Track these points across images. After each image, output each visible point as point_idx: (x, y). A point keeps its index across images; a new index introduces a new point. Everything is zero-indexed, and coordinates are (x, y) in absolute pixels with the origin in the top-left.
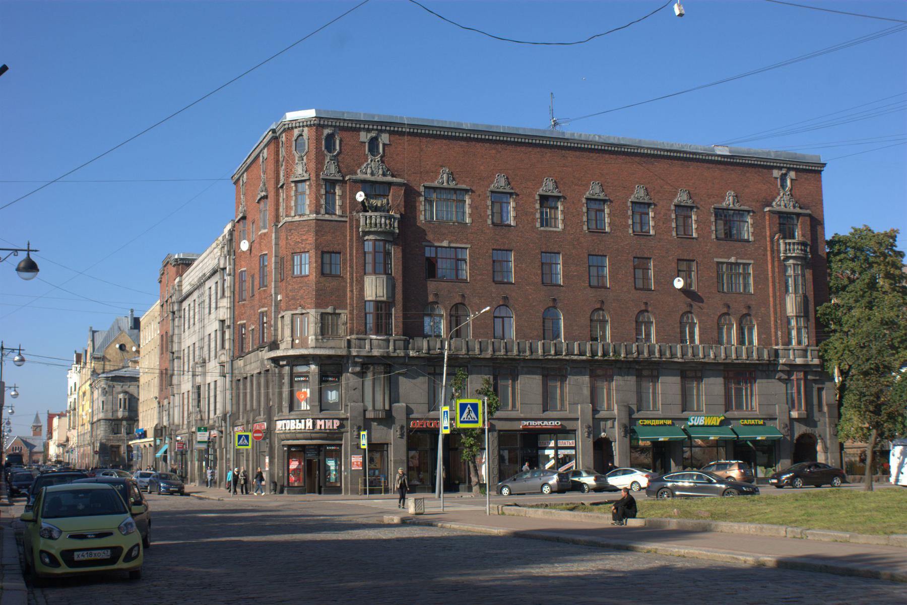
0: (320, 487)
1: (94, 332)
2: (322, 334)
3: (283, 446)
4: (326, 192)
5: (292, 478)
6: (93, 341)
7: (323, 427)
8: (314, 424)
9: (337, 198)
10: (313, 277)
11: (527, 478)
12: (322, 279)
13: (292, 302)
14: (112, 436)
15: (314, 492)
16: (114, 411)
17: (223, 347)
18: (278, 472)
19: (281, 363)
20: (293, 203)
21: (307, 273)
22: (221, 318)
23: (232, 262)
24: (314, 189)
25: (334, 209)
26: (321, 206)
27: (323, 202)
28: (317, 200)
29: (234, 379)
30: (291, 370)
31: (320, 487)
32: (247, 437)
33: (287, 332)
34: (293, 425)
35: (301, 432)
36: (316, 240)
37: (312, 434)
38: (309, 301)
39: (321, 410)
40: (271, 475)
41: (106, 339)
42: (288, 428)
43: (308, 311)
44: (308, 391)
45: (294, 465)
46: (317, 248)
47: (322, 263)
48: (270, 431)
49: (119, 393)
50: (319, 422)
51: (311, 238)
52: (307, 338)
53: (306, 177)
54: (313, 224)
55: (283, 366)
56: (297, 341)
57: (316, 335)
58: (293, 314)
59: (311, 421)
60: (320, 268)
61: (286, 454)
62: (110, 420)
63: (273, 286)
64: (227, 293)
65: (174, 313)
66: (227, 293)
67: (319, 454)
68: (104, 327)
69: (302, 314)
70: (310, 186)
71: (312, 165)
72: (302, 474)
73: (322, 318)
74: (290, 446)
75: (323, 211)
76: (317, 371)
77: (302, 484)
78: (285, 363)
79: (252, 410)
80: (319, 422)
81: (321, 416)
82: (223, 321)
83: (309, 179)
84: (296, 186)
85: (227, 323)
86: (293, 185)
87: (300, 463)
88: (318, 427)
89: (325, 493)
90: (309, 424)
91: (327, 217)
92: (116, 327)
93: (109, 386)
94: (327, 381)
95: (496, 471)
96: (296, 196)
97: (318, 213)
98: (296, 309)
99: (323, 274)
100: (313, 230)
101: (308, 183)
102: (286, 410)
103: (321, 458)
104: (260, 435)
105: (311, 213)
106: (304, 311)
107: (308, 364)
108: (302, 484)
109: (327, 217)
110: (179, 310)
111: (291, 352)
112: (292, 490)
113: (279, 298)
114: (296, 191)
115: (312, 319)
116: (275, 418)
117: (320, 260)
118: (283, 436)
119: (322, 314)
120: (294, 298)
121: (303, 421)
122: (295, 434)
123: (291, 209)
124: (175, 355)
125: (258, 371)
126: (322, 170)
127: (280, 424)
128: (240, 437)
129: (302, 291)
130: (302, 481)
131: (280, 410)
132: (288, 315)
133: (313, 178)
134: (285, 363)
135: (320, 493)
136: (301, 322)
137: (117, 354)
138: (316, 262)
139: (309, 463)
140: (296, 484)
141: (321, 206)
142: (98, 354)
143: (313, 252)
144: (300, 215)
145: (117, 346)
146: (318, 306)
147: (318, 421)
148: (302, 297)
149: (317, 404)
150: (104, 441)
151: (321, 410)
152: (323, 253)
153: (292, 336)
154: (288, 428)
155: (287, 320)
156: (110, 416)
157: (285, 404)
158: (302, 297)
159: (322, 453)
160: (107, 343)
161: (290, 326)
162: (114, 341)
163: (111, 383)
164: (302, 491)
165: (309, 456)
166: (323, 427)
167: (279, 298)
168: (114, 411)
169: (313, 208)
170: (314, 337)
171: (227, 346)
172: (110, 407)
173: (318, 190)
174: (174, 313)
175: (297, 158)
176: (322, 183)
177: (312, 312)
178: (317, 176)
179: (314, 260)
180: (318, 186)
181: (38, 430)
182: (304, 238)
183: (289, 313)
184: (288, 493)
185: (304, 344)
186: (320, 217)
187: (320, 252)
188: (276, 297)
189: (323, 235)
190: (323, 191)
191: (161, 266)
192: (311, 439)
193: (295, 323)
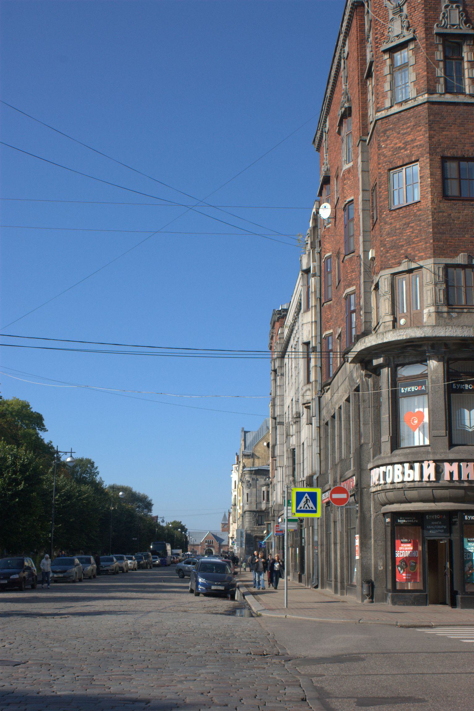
0: (454, 594)
1: (246, 432)
2: (448, 303)
3: (384, 514)
4: (446, 57)
5: (402, 575)
6: (245, 440)
7: (456, 477)
8: (439, 472)
9: (466, 65)
10: (427, 204)
11: (122, 570)
12: (445, 205)
13: (392, 253)
14: (256, 527)
15: (444, 603)
16: (258, 503)
17: (308, 382)
18: (377, 563)
19: (375, 362)
20: (387, 87)
21: (417, 198)
22: (305, 340)
23: (317, 256)
24: (423, 53)
25: (460, 79)
26: (436, 80)
27: (440, 72)
28: (430, 69)
29: (323, 423)
30: (394, 374)
31: (454, 594)
32: (313, 496)
33: (385, 306)
34: (400, 474)
35: (413, 486)
36: (430, 137)
37: (433, 490)
38: (422, 245)
39: (451, 445)
40: (365, 569)
41: (255, 438)
42: (389, 480)
43: (421, 263)
44: (426, 411)
45: (404, 550)
46: (432, 152)
47: (444, 179)
48: (361, 490)
49: (263, 486)
50: (447, 468)
51: (421, 137)
52: (421, 313)
53: (408, 36)
54: (424, 111)
55: (380, 366)
56: (402, 321)
57: (436, 304)
58: (394, 274)
59: (433, 465)
60: (439, 185)
61: (389, 529)
62: (254, 511)
63: (361, 239)
64: (312, 302)
65: (275, 371)
66: (312, 302)
67: (450, 531)
68: (254, 428)
69: (410, 271)
70: (416, 51)
71: (419, 16)
72: (419, 568)
73: (446, 274)
74: (395, 515)
75: (440, 88)
76: (440, 373)
77: (420, 587)
78: (381, 360)
79: (341, 460)
80: (447, 468)
81: (451, 456)
82: (307, 344)
83: (413, 39)
84: (392, 58)
85: (313, 344)
86: (386, 56)
87: (415, 548)
88: (447, 477)
89: (462, 607)
90: (430, 470)
91: (448, 98)
92: (265, 428)
93: (253, 479)
94: (461, 391)
95: (89, 580)
96: (391, 73)
97: (431, 91)
98: (399, 264)
99: (445, 196)
100: (424, 121)
101: (412, 46)
102: (386, 447)
103: (455, 537)
104: (344, 496)
105: (418, 93)
106: (413, 266)
107: (423, 361)
108: (420, 587)
109: (448, 98)
110: (281, 367)
111: (391, 337)
112: (400, 596)
113: (371, 254)
114: (392, 65)
115: (427, 276)
116: (370, 466)
117: (439, 172)
118: (382, 497)
119: (447, 267)
120: (395, 246)
121: (417, 465)
122: (403, 491)
123: (384, 97)
124: (278, 421)
125: (346, 397)
126: (436, 19)
127: (376, 475)
128: (300, 496)
129: (408, 231)
130: (419, 579)
131: (377, 450)
132: (383, 278)
133: (421, 34)
134: (381, 360)
135: (454, 604)
136: (409, 285)
137: (265, 451)
138: (432, 174)
139: (432, 548)
140: (410, 586)
141: (436, 80)
142: (248, 452)
143: (425, 160)
144: (401, 104)
145: (265, 444)
146: (437, 252)
147: (446, 465)
148: (409, 242)
149: (443, 432)
150: (249, 532)
151: (451, 445)
152: (444, 159)
153: (393, 313)
154: (389, 480)
155: (385, 287)
156: (254, 508)
157: (386, 438)
158: (409, 242)
159: (456, 528)
160: (256, 442)
161: (389, 296)
162: (262, 439)
163: (254, 476)
164: (420, 598)
165: (433, 533)
166: (456, 477)
167: (371, 254)
168: (258, 503)
169: (423, 84)
170: (432, 309)
171: (312, 378)
172: (254, 499)
173: (430, 54)
174: (275, 371)
175: (391, 12)
176: (437, 40)
177: (429, 263)
178: (428, 29)
179: (428, 172)
180: (430, 47)
181: (226, 527)
182: (409, 138)
183: (387, 273)
184: (394, 603)
185: (415, 320)
186: (435, 98)
187: (438, 159)
188: (366, 252)
189: (443, 129)
190: (439, 55)
191: (269, 327)
192: (434, 500)
193: (397, 292)
